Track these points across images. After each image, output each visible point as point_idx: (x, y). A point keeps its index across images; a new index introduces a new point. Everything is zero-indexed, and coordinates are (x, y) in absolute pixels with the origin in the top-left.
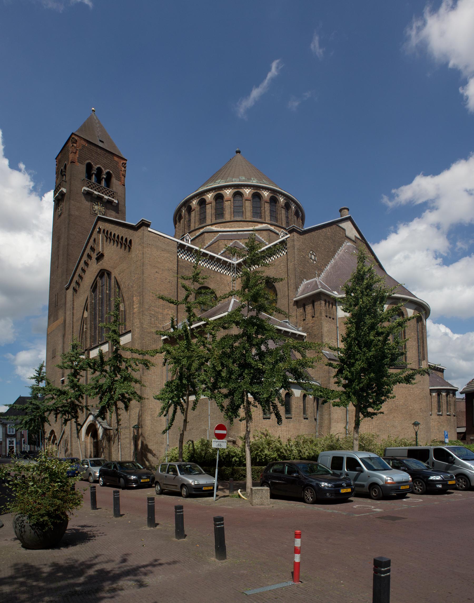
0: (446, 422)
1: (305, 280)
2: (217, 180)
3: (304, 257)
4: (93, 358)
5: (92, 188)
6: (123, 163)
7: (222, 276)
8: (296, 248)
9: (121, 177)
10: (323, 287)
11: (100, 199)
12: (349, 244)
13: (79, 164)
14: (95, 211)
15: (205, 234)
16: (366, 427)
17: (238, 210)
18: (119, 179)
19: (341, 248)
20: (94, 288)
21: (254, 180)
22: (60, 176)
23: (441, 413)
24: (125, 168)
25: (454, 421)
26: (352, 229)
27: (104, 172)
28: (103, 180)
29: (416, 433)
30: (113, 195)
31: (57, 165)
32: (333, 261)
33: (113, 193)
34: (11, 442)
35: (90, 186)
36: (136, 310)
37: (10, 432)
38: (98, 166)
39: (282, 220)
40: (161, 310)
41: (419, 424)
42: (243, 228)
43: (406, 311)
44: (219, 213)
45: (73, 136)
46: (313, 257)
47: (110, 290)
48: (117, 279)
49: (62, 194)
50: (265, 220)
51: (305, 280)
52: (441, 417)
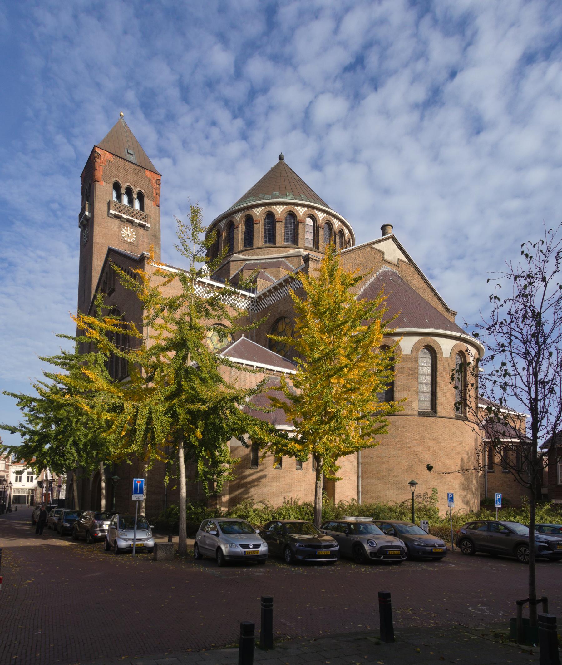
4: (404, 355)
5: (119, 212)
13: (104, 184)
15: (231, 263)
16: (382, 485)
21: (289, 195)
29: (413, 493)
30: (145, 219)
38: (127, 184)
41: (416, 484)
42: (272, 255)
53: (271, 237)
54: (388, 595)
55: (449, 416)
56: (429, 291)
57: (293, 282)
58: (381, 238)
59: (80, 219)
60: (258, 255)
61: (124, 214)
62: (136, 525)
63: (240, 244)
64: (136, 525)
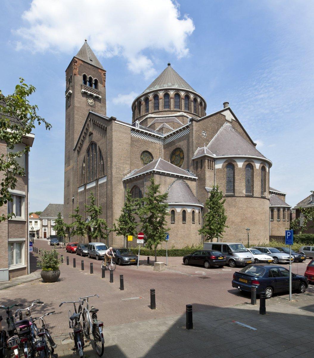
0: (282, 225)
1: (199, 148)
2: (156, 85)
3: (199, 135)
5: (86, 90)
6: (104, 73)
7: (156, 144)
8: (194, 130)
9: (103, 82)
10: (208, 152)
11: (91, 96)
12: (228, 124)
13: (79, 76)
14: (89, 103)
17: (167, 105)
18: (102, 83)
19: (222, 127)
20: (88, 151)
21: (176, 85)
22: (68, 82)
23: (284, 220)
24: (105, 76)
25: (288, 224)
26: (230, 115)
27: (94, 80)
28: (93, 84)
30: (99, 94)
31: (66, 75)
32: (216, 136)
33: (99, 92)
34: (45, 230)
35: (85, 88)
36: (109, 165)
37: (44, 224)
38: (90, 76)
39: (191, 109)
40: (122, 165)
43: (255, 165)
44: (157, 106)
45: (75, 59)
46: (204, 134)
47: (96, 153)
48: (100, 147)
49: (70, 94)
50: (181, 110)
51: (199, 148)
52: (279, 222)
53: (167, 105)
54: (154, 291)
55: (259, 197)
56: (245, 134)
57: (184, 131)
58: (223, 109)
59: (66, 94)
60: (162, 115)
61: (89, 91)
62: (139, 253)
63: (151, 109)
64: (139, 253)
